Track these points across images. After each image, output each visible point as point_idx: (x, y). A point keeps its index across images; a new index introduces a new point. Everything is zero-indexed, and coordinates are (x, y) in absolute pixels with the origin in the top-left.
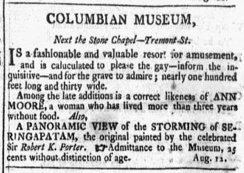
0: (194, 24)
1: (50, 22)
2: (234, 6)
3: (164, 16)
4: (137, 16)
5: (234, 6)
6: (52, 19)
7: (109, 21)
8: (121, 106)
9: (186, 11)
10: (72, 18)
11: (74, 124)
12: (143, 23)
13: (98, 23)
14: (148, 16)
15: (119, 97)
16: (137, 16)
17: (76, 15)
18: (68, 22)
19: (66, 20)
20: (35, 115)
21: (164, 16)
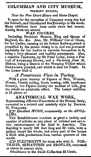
0: (81, 8)
1: (49, 8)
2: (82, 3)
3: (71, 6)
4: (62, 6)
5: (82, 3)
6: (9, 7)
7: (28, 7)
8: (43, 135)
9: (79, 4)
10: (16, 6)
11: (25, 144)
12: (64, 8)
13: (24, 8)
14: (65, 6)
15: (57, 76)
16: (62, 6)
17: (17, 6)
18: (14, 7)
19: (14, 7)
20: (25, 64)
21: (71, 6)
